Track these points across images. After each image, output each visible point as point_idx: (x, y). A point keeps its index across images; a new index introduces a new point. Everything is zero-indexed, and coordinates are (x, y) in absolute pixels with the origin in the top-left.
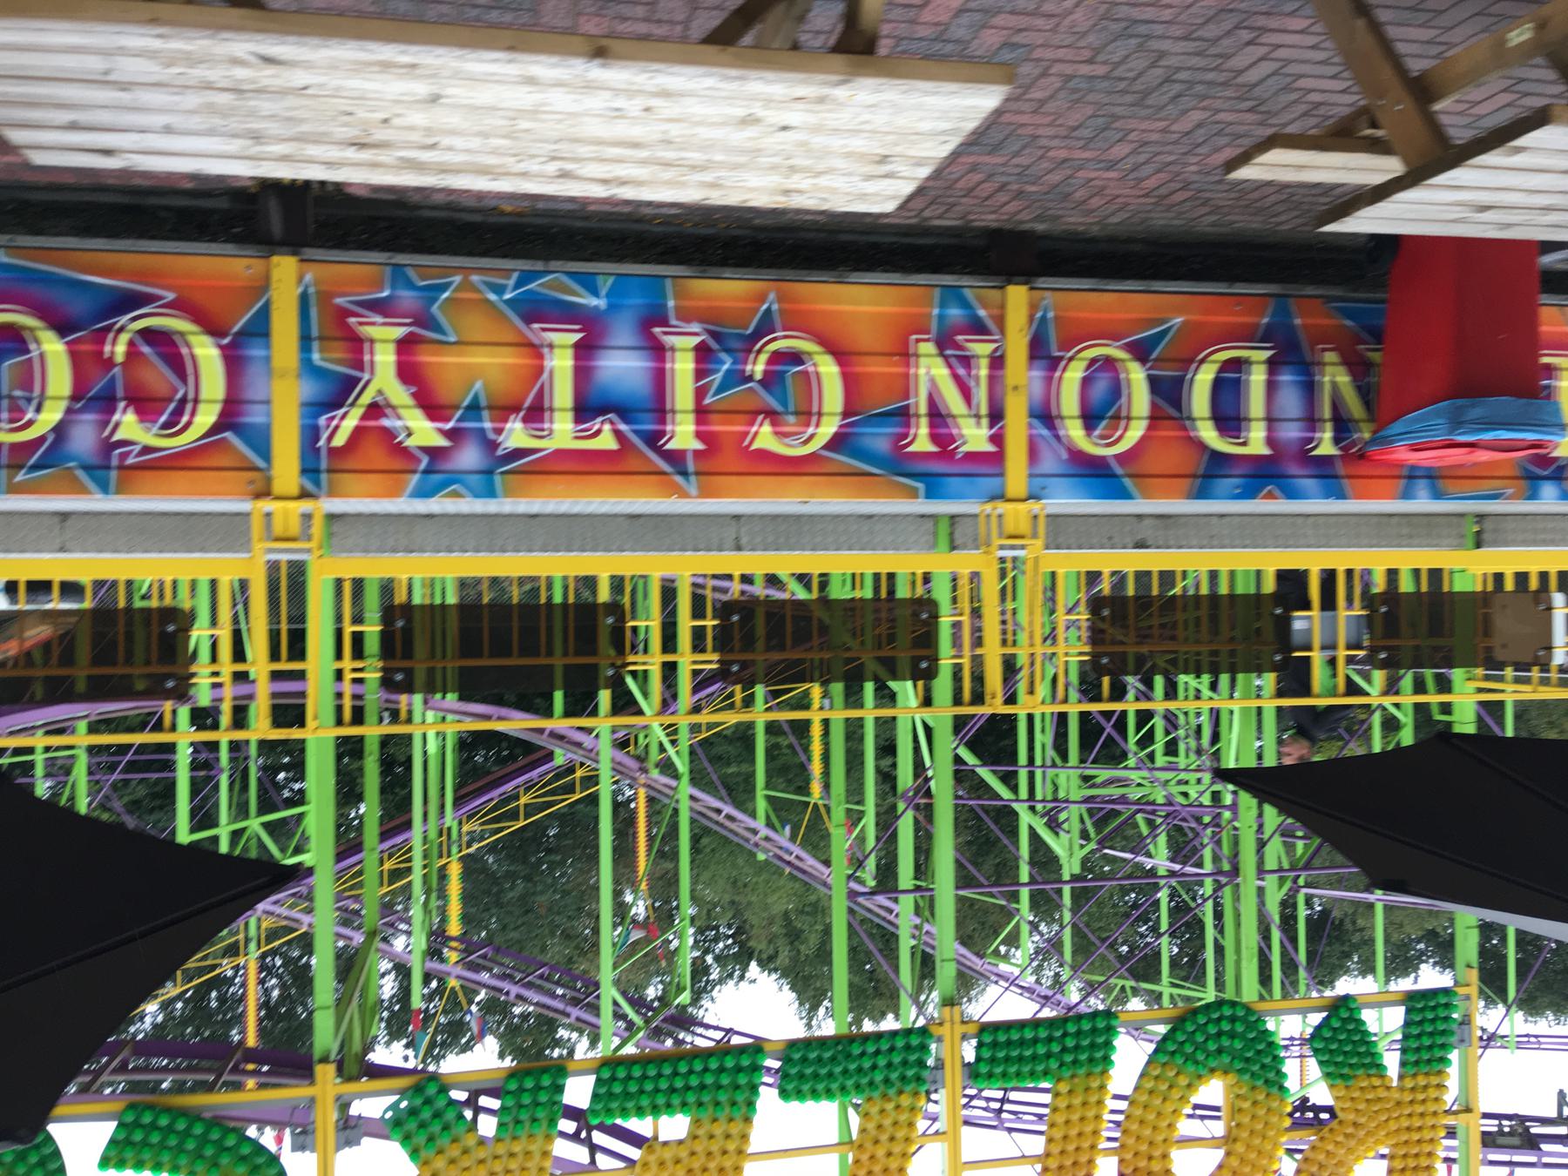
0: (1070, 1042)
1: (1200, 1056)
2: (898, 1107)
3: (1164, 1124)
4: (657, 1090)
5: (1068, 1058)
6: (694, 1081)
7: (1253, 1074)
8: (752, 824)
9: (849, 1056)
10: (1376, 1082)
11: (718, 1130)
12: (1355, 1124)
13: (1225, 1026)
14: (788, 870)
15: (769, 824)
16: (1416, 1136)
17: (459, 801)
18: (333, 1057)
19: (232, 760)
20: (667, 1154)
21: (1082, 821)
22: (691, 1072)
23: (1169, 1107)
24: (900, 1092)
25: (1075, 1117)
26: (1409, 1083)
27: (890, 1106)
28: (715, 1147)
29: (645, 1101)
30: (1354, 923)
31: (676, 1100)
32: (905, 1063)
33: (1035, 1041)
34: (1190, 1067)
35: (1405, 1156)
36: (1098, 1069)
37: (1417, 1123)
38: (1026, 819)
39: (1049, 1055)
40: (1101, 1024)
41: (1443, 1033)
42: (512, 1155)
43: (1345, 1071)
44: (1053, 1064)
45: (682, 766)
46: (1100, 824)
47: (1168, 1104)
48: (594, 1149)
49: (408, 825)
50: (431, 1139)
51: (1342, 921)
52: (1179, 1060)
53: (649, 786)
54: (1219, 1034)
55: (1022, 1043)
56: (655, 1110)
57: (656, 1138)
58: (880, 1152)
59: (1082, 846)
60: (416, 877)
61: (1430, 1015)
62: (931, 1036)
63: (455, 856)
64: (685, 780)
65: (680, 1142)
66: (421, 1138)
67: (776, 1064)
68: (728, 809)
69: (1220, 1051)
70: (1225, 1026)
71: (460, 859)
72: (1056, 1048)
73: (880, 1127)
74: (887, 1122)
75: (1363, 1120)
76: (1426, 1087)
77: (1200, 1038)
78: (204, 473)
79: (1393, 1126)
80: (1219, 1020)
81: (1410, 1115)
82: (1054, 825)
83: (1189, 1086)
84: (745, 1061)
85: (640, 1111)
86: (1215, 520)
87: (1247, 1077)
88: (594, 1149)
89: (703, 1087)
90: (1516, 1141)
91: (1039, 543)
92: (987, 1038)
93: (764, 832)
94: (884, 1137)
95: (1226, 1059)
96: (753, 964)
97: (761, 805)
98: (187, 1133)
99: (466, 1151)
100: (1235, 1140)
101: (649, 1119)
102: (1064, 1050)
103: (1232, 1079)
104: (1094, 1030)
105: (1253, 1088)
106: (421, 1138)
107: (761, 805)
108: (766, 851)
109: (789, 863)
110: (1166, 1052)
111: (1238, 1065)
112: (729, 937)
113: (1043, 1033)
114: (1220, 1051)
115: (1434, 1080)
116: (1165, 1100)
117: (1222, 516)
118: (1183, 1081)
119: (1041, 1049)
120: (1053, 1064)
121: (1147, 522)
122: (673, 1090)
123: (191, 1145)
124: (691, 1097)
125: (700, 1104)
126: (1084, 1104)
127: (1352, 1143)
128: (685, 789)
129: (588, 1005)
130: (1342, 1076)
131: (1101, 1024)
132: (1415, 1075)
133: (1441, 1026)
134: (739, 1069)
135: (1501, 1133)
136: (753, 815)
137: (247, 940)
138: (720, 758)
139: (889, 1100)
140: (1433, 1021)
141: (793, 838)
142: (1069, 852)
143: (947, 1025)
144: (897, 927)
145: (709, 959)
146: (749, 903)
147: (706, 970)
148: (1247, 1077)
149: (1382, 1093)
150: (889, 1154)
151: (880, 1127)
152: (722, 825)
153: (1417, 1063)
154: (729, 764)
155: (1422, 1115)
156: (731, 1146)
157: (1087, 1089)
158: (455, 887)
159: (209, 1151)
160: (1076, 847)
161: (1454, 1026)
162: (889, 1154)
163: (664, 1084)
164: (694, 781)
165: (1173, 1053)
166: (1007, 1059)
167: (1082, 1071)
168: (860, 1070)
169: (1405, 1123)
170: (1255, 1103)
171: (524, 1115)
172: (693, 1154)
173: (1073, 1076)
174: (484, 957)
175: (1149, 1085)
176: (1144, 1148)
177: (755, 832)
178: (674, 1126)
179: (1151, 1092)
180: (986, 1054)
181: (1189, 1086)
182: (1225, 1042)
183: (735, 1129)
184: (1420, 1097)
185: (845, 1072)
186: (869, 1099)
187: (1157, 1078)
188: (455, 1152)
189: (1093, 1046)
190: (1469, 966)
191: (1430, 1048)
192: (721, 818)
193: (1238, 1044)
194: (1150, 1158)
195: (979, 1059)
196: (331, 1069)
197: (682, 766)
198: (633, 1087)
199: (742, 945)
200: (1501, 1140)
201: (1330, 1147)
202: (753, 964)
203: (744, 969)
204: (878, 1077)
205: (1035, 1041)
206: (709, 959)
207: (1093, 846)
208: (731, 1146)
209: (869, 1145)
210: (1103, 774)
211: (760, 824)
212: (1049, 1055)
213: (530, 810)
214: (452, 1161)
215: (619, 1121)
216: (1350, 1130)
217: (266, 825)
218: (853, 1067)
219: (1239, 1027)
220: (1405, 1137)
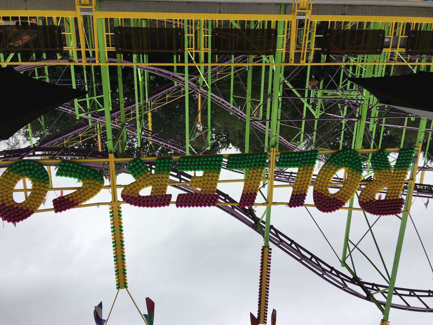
0: (304, 158)
1: (340, 163)
2: (257, 171)
3: (327, 179)
4: (195, 164)
5: (304, 162)
6: (205, 163)
7: (353, 168)
8: (229, 104)
9: (245, 159)
10: (387, 171)
11: (210, 174)
12: (380, 181)
13: (348, 155)
14: (239, 118)
15: (234, 105)
16: (396, 185)
17: (149, 97)
18: (113, 152)
19: (87, 81)
20: (198, 179)
21: (321, 106)
22: (204, 160)
23: (329, 175)
24: (258, 168)
25: (304, 176)
26: (396, 172)
27: (255, 171)
28: (210, 178)
29: (192, 167)
30: (397, 138)
31: (200, 167)
32: (260, 161)
33: (295, 157)
34: (336, 165)
35: (392, 190)
36: (311, 165)
37: (397, 182)
38: (306, 105)
39: (298, 161)
40: (313, 153)
41: (409, 159)
42: (159, 177)
43: (379, 168)
44: (299, 163)
45: (209, 87)
46: (325, 107)
47: (329, 174)
48: (181, 179)
49: (134, 103)
50: (139, 173)
51: (394, 137)
52: (334, 163)
53: (201, 93)
54: (346, 157)
55: (292, 157)
56: (195, 169)
57: (195, 176)
58: (252, 182)
59: (320, 112)
60: (138, 116)
61: (406, 155)
62: (267, 155)
63: (150, 111)
64: (210, 91)
65: (201, 177)
66: (136, 172)
67: (227, 160)
68: (222, 100)
69: (345, 161)
70: (348, 155)
71: (151, 112)
72: (300, 159)
73: (252, 176)
74: (254, 175)
75: (382, 180)
76: (401, 173)
77: (340, 158)
78: (279, 206)
79: (390, 182)
80: (346, 154)
81: (395, 180)
82: (314, 106)
83: (335, 170)
84: (218, 159)
85: (191, 170)
86: (368, 7)
87: (352, 168)
88: (181, 179)
89: (207, 164)
90: (427, 191)
91: (310, 12)
92: (282, 156)
93: (232, 106)
94: (253, 179)
95: (346, 163)
96: (230, 144)
97: (232, 99)
98: (77, 168)
99: (147, 176)
100: (346, 184)
101: (193, 172)
102: (303, 159)
103: (347, 168)
104: (311, 155)
105: (353, 171)
106: (136, 172)
107: (232, 99)
108: (232, 112)
109: (239, 115)
110: (330, 161)
111: (349, 165)
112: (224, 137)
113: (297, 155)
114: (345, 161)
115: (404, 171)
116: (328, 173)
117: (370, 6)
118: (334, 168)
119: (296, 159)
120: (299, 163)
121: (347, 7)
122: (199, 165)
123: (79, 171)
124: (204, 167)
125: (206, 168)
126: (307, 173)
127: (378, 186)
128: (210, 93)
129: (184, 148)
130: (378, 169)
131: (313, 153)
132: (399, 170)
133: (408, 158)
134: (216, 160)
135: (424, 189)
136: (230, 103)
137: (97, 130)
138: (222, 88)
139: (255, 170)
140: (407, 156)
141: (241, 110)
142: (317, 114)
143: (272, 152)
144: (265, 132)
145: (219, 142)
146: (229, 128)
147: (218, 145)
148: (352, 168)
149: (388, 174)
150: (254, 182)
151: (252, 176)
152: (220, 104)
153: (400, 167)
154: (225, 89)
155: (399, 180)
156: (214, 179)
157: (308, 169)
158: (150, 119)
159: (83, 173)
160: (319, 112)
161: (412, 158)
162: (254, 182)
163: (197, 163)
164: (212, 92)
165: (332, 161)
166: (287, 161)
167: (307, 165)
168: (248, 162)
169: (394, 182)
170: (353, 175)
171: (161, 168)
172: (204, 180)
173: (304, 166)
174: (156, 135)
175: (325, 169)
176: (321, 184)
177: (229, 106)
178: (200, 173)
179: (325, 171)
180: (282, 160)
181: (335, 170)
182: (347, 159)
183: (215, 175)
184: (399, 175)
185: (244, 163)
186: (250, 169)
187: (327, 167)
188: (145, 176)
189: (311, 159)
190: (420, 142)
191: (404, 163)
192: (220, 102)
193: (350, 160)
194: (323, 187)
195: (279, 161)
196: (113, 155)
197: (209, 87)
198: (189, 164)
199: (228, 139)
200: (423, 191)
201: (372, 186)
202: (230, 144)
203: (228, 145)
204: (253, 164)
205: (295, 157)
206: (219, 142)
207: (323, 112)
208: (214, 179)
209: (249, 180)
210: (330, 92)
211: (231, 105)
212: (298, 161)
213: (169, 99)
214: (144, 178)
215: (185, 172)
216: (378, 183)
217: (97, 99)
218: (246, 161)
219: (351, 156)
220: (393, 185)
